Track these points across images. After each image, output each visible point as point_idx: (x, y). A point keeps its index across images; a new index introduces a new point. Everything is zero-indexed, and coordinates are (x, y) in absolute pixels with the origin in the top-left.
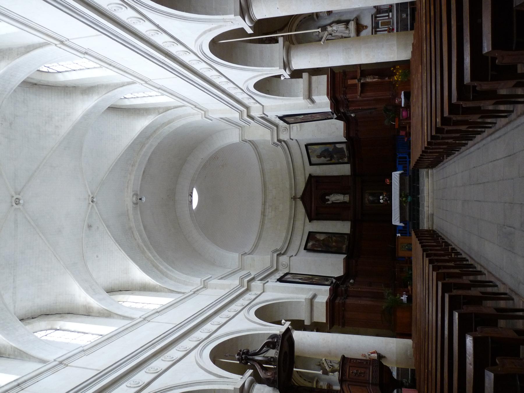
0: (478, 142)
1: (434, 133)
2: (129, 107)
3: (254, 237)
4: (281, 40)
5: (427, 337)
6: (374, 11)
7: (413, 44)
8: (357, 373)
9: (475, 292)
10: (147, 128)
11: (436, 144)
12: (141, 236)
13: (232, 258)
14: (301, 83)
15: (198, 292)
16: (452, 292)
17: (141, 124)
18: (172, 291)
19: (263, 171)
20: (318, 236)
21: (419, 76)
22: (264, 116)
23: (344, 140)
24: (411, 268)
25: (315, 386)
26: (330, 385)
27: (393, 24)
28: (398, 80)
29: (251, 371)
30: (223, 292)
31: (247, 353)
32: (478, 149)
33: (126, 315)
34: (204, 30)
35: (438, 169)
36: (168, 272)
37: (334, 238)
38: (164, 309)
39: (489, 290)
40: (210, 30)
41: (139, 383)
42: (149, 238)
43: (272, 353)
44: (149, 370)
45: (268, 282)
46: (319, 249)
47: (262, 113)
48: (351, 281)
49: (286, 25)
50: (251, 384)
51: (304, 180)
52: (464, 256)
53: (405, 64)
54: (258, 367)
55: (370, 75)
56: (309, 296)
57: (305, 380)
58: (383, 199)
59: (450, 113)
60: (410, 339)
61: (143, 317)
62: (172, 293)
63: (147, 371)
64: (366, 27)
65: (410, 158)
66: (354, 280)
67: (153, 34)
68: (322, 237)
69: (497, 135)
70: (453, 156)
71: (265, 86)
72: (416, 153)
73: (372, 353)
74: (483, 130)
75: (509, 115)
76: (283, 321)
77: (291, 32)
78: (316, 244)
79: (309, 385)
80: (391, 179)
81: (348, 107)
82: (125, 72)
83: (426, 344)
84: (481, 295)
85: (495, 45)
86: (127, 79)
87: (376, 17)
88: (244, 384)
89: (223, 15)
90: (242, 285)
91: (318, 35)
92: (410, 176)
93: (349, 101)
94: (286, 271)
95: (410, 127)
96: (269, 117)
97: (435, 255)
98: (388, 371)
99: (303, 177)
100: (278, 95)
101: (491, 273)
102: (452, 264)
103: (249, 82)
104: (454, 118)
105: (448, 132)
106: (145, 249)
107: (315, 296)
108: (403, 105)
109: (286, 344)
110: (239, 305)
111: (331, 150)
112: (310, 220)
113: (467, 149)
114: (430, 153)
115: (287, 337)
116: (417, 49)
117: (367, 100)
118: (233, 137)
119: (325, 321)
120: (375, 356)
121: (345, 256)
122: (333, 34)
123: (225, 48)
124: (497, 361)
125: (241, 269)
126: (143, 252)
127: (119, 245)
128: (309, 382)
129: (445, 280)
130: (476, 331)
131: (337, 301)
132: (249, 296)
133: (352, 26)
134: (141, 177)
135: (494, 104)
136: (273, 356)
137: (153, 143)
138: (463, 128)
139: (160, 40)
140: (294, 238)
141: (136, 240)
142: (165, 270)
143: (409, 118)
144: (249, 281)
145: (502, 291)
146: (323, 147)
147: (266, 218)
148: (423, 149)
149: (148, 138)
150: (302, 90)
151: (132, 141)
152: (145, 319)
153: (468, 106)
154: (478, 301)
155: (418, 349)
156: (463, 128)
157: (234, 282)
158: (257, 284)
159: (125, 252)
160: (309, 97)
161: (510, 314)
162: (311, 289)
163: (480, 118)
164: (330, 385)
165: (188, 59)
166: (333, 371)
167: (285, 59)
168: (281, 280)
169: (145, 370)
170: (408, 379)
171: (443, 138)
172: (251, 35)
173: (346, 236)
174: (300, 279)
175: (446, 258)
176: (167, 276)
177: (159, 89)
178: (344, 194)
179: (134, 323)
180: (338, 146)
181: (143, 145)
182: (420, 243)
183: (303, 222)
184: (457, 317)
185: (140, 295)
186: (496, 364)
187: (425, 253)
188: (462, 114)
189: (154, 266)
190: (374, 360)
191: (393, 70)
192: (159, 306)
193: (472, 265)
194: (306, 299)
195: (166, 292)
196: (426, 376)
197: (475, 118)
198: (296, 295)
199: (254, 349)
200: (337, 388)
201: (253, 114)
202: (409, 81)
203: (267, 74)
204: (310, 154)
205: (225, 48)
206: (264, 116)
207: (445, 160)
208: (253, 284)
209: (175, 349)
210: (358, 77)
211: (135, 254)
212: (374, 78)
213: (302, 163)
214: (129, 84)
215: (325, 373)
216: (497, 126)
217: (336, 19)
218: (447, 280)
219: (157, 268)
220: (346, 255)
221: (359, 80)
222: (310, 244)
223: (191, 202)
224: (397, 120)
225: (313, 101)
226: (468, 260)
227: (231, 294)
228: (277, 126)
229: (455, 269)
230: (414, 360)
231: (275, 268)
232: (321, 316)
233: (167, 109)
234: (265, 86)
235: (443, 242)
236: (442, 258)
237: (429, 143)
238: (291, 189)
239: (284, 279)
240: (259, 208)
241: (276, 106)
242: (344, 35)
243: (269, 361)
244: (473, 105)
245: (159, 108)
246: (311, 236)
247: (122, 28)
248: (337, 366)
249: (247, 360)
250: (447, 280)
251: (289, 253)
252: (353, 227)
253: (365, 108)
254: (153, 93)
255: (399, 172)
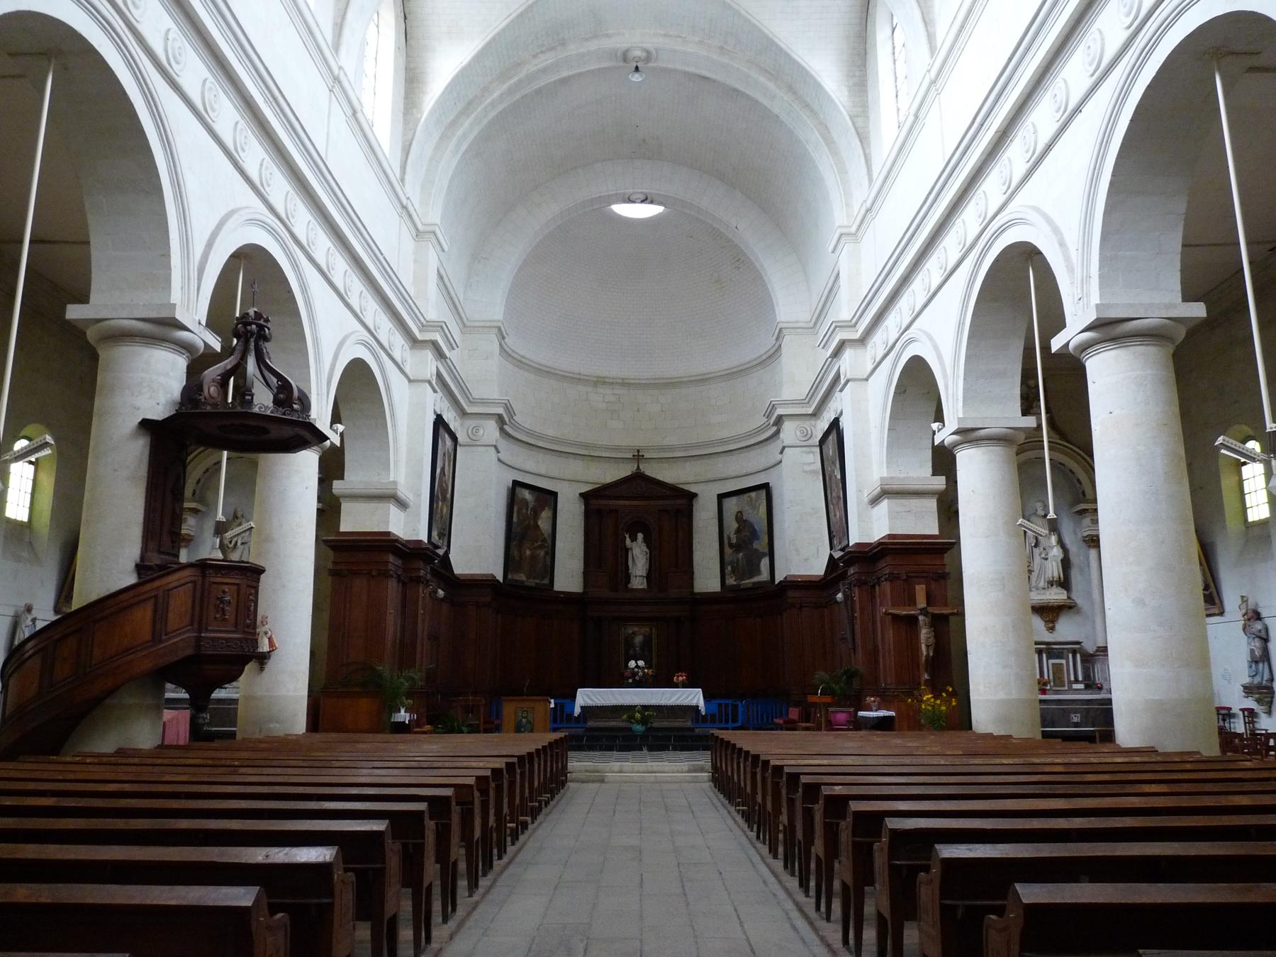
0: (780, 882)
1: (804, 779)
2: (869, 41)
3: (542, 357)
4: (1030, 422)
5: (316, 764)
6: (1090, 648)
7: (1010, 736)
8: (222, 602)
9: (431, 870)
10: (818, 86)
11: (776, 785)
12: (544, 71)
13: (490, 304)
14: (920, 472)
15: (406, 218)
16: (431, 819)
17: (827, 71)
18: (406, 151)
19: (703, 380)
20: (546, 514)
21: (936, 749)
22: (843, 381)
23: (779, 578)
24: (474, 730)
25: (186, 505)
26: (188, 540)
27: (1057, 692)
28: (922, 701)
29: (217, 346)
30: (407, 280)
31: (262, 336)
32: (764, 882)
33: (347, 32)
34: (1063, 230)
35: (711, 794)
36: (454, 141)
37: (542, 553)
38: (362, 130)
39: (437, 906)
40: (1062, 244)
41: (178, 63)
42: (538, 92)
43: (263, 399)
44: (210, 89)
45: (435, 391)
46: (515, 515)
47: (849, 376)
48: (441, 593)
49: (1063, 435)
50: (186, 347)
51: (682, 480)
52: (511, 850)
53: (961, 718)
54: (228, 363)
55: (935, 637)
56: (404, 492)
57: (198, 482)
58: (637, 666)
59: (858, 814)
60: (308, 730)
61: (342, 77)
62: (403, 149)
63: (208, 84)
64: (1052, 629)
65: (734, 729)
66: (442, 600)
67: (1058, 98)
68: (544, 523)
69: (801, 923)
70: (745, 826)
71: (917, 383)
72: (748, 741)
73: (270, 639)
74: (812, 892)
75: (849, 950)
76: (340, 428)
77: (1050, 449)
78: (527, 510)
79: (188, 492)
80: (685, 685)
81: (861, 584)
82: (962, 27)
83: (301, 764)
84: (425, 885)
85: (1034, 911)
86: (944, 31)
87: (1074, 652)
88: (185, 329)
89: (1101, 276)
90: (423, 327)
91: (1035, 514)
92: (692, 730)
93: (873, 587)
94: (461, 437)
95: (807, 729)
96: (837, 394)
97: (512, 784)
98: (232, 677)
99: (691, 479)
100: (893, 417)
101: (474, 909)
102: (492, 821)
103: (928, 343)
104: (845, 826)
105: (808, 815)
106: (512, 81)
107: (402, 505)
108: (861, 713)
109: (288, 432)
110: (378, 320)
111: (756, 545)
112: (585, 496)
113: (762, 858)
114: (754, 775)
115: (307, 435)
116: (999, 745)
117: (874, 631)
118: (790, 306)
119: (342, 529)
120: (264, 647)
121: (500, 578)
122: (1036, 551)
123: (1018, 280)
124: (280, 915)
125: (464, 325)
126: (503, 76)
127: (521, 15)
128: (194, 494)
129: (458, 804)
130: (346, 870)
131: (391, 558)
132: (398, 344)
133: (1056, 596)
134: (692, 70)
135: (880, 916)
136: (256, 401)
137: (778, 102)
138: (818, 848)
139: (1043, 117)
140: (541, 456)
141: (535, 56)
142: (459, 133)
143: (831, 726)
144: (434, 344)
145: (435, 933)
146: (761, 526)
147: (590, 389)
148: (762, 758)
149: (791, 89)
150: (902, 476)
151: (783, 46)
152: (337, 79)
153: (876, 855)
154: (413, 876)
155: (283, 747)
156: (818, 848)
157: (433, 308)
158: (427, 365)
159: (504, 30)
160: (886, 493)
161: (423, 924)
162: (419, 496)
163: (844, 885)
164: (188, 540)
165: (992, 189)
166: (222, 547)
167: (982, 432)
168: (439, 423)
169: (211, 79)
170: (209, 724)
171: (791, 802)
172: (1046, 347)
173: (546, 581)
174: (443, 469)
175: (506, 810)
176: (444, 138)
177: (916, 116)
178: (648, 577)
179: (324, 53)
180: (765, 562)
181: (775, 76)
182: (537, 750)
183: (579, 478)
184: (375, 828)
185: (396, 71)
186: (272, 913)
187: (515, 760)
188: (854, 844)
189: (470, 103)
190: (255, 643)
191: (947, 692)
192: (369, 116)
193: (491, 867)
194: (395, 483)
195: (404, 135)
196: (223, 762)
197: (843, 871)
198: (404, 461)
199: (272, 355)
200: (184, 557)
201: (848, 354)
202: (920, 727)
203: (947, 388)
204: (746, 496)
205: (1018, 280)
206: (843, 381)
207: (732, 809)
208: (429, 355)
209: (265, 156)
210: (931, 610)
211: (499, 56)
212: (928, 646)
213: (724, 476)
214: (931, 38)
215: (220, 529)
216: (822, 924)
217: (1073, 558)
218: (456, 810)
219: (464, 112)
220: (501, 580)
221: (924, 612)
222: (527, 495)
223: (630, 200)
224: (827, 699)
225: (875, 501)
226: (500, 858)
227: (404, 301)
228: (816, 415)
229: (479, 830)
230: (257, 736)
231: (469, 410)
232: (354, 520)
233: (863, 138)
234: (917, 383)
235: (540, 802)
236: (506, 800)
237: (779, 769)
238: (663, 449)
239: (442, 431)
240: (613, 370)
241: (866, 412)
242: (1034, 575)
243: (243, 392)
244: (877, 870)
245: (867, 117)
246: (548, 498)
247: (1076, 16)
248: (235, 556)
249: (244, 336)
250: (456, 810)
251: (503, 444)
252: (568, 597)
253: (858, 628)
254: (904, 103)
255: (701, 703)
